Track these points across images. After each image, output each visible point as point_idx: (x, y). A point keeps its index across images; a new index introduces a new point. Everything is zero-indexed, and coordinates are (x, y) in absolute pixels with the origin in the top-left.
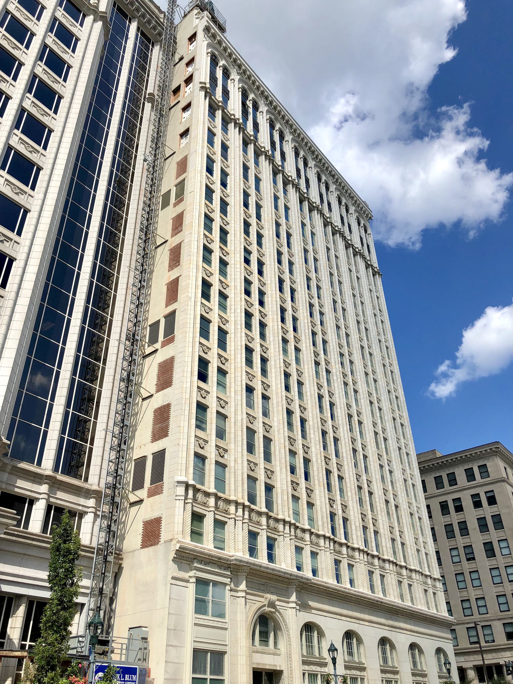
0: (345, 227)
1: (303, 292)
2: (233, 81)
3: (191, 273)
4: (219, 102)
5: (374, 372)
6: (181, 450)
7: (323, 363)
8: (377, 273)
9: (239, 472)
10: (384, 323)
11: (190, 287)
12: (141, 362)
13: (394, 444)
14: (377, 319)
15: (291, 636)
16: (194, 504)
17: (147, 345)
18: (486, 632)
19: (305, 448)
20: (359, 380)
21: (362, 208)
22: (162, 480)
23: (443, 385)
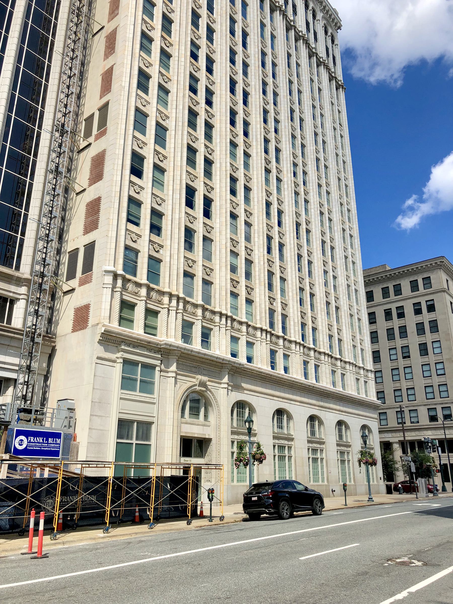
0: (310, 34)
1: (258, 96)
3: (126, 60)
5: (328, 184)
6: (109, 241)
7: (274, 171)
8: (341, 87)
9: (174, 268)
10: (343, 138)
11: (124, 76)
12: (76, 157)
13: (341, 252)
14: (336, 133)
15: (222, 411)
16: (184, 314)
17: (82, 139)
18: (413, 415)
19: (248, 250)
20: (311, 191)
21: (330, 16)
22: (91, 270)
23: (409, 218)
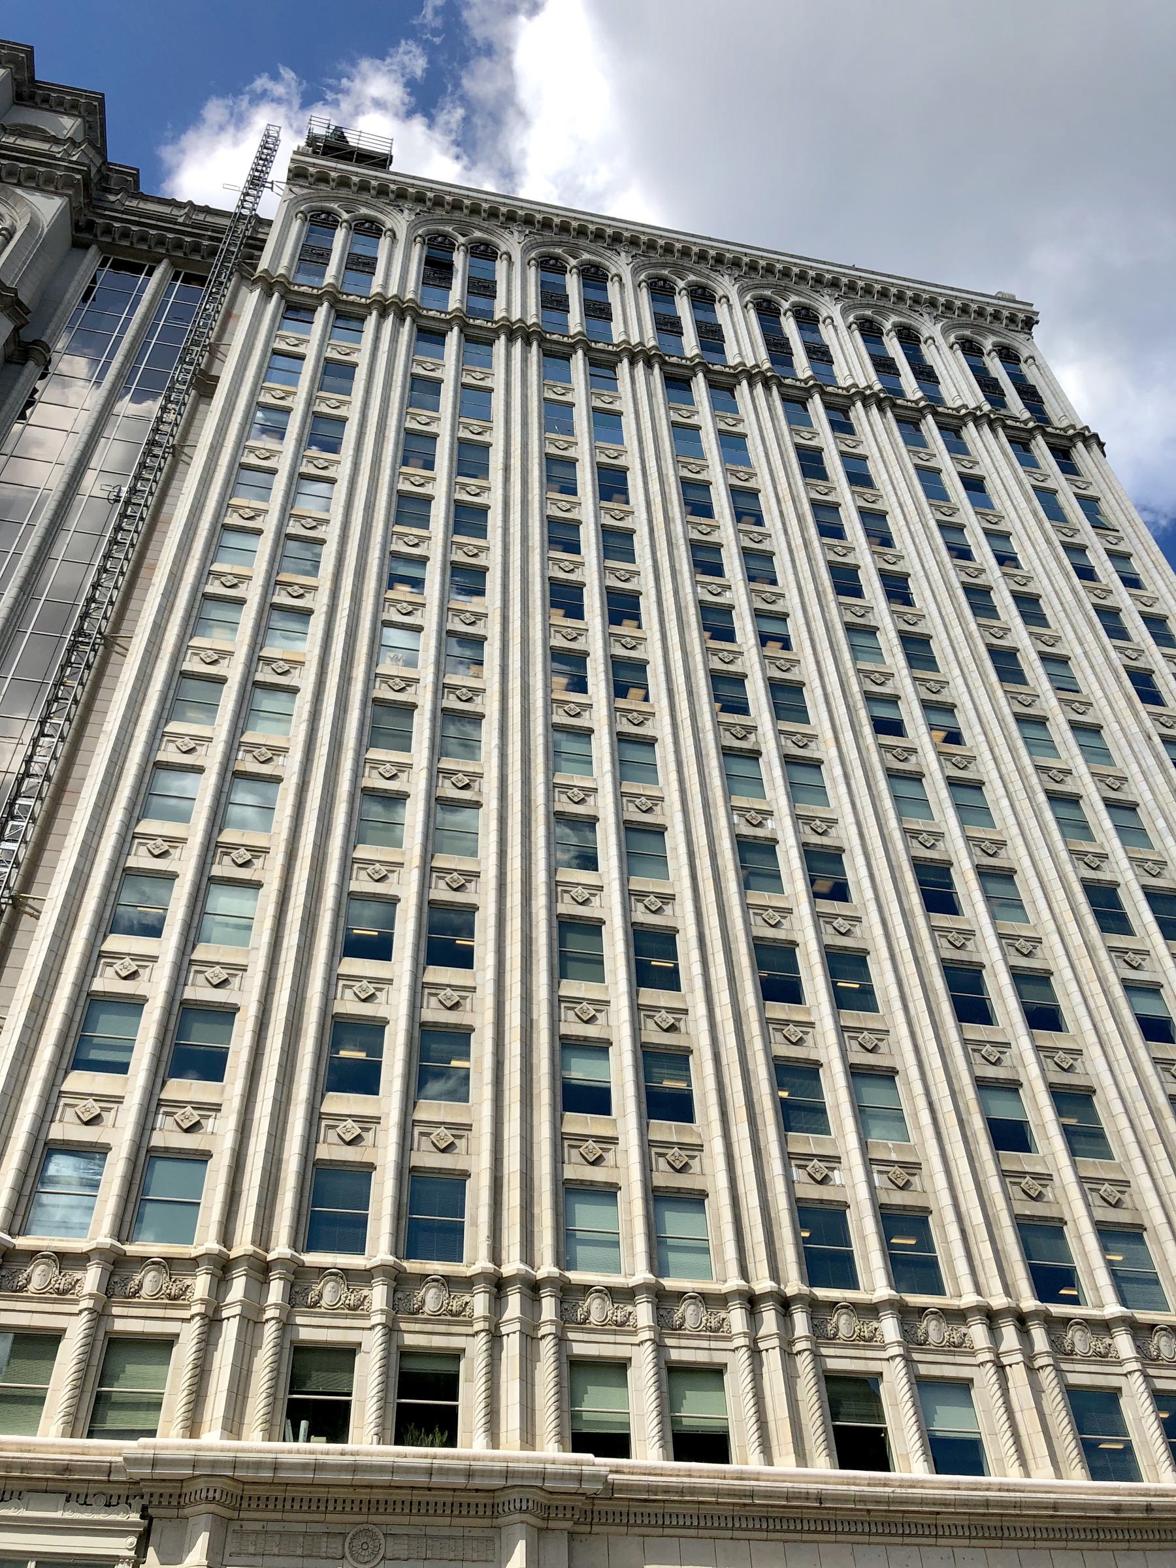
4: (1026, 422)
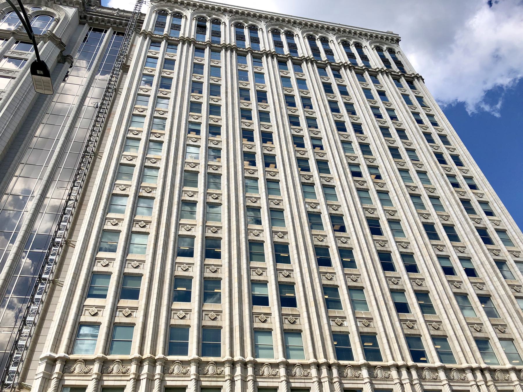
2: (399, 53)
16: (496, 384)
